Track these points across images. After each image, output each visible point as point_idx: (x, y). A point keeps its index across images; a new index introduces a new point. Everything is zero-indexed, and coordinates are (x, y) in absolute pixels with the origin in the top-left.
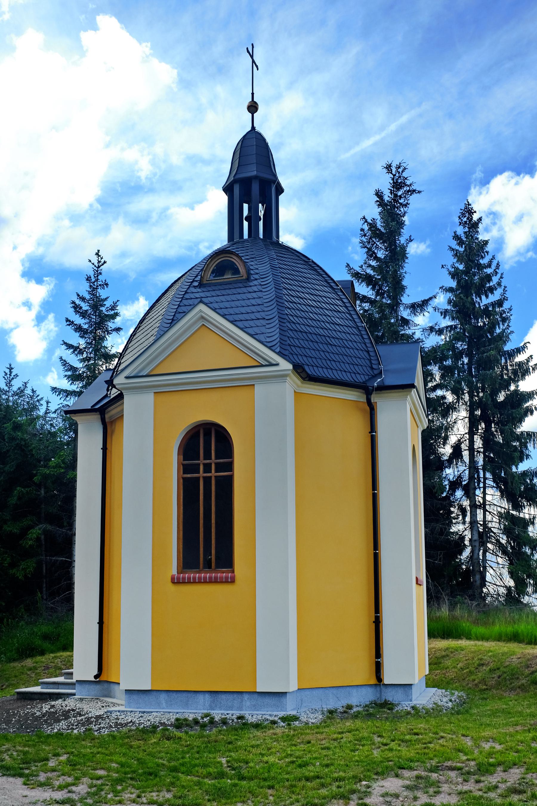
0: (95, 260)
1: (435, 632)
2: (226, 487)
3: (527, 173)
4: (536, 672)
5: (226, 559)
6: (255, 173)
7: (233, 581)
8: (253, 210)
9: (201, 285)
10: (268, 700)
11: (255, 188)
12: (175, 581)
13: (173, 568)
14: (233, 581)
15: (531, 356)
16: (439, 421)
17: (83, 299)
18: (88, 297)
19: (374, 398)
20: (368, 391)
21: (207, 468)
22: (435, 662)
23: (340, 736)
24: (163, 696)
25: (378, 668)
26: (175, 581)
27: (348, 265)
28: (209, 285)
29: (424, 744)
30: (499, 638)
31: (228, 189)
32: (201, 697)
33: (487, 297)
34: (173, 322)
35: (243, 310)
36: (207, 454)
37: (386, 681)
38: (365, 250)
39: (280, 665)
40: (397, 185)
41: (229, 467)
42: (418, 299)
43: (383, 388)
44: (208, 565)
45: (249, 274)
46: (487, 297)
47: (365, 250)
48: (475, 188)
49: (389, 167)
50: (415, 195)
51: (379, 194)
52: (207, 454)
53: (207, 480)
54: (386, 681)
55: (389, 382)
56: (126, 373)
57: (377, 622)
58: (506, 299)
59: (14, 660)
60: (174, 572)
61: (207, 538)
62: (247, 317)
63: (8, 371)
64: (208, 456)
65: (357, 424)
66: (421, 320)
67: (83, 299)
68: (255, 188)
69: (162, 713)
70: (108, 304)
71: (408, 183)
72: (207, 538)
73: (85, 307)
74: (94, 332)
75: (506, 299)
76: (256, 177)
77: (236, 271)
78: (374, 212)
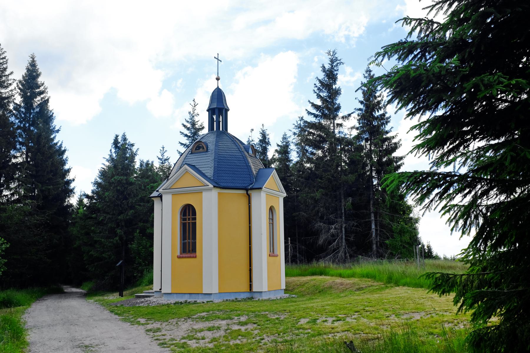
0: (193, 103)
1: (287, 275)
2: (194, 224)
5: (194, 250)
6: (216, 106)
7: (196, 257)
8: (218, 118)
9: (191, 154)
10: (206, 296)
11: (217, 111)
12: (179, 257)
13: (178, 253)
14: (196, 257)
15: (401, 140)
17: (188, 122)
18: (190, 121)
19: (249, 192)
20: (247, 190)
22: (287, 284)
24: (175, 295)
25: (251, 286)
26: (179, 257)
27: (309, 101)
28: (194, 153)
30: (363, 276)
31: (208, 111)
32: (186, 295)
33: (378, 111)
34: (181, 167)
35: (203, 164)
36: (188, 213)
38: (316, 94)
39: (211, 284)
40: (332, 61)
41: (195, 219)
42: (346, 113)
43: (252, 189)
44: (189, 251)
45: (207, 149)
46: (378, 111)
47: (316, 94)
48: (284, 150)
49: (329, 53)
50: (342, 65)
51: (323, 67)
52: (188, 213)
54: (254, 290)
55: (255, 187)
56: (162, 188)
58: (386, 113)
59: (147, 285)
61: (189, 244)
62: (204, 166)
63: (162, 149)
64: (189, 215)
65: (245, 201)
67: (188, 122)
68: (217, 111)
69: (172, 300)
70: (199, 123)
71: (339, 59)
72: (189, 244)
73: (189, 125)
74: (193, 136)
75: (386, 113)
76: (216, 108)
77: (203, 149)
78: (322, 76)
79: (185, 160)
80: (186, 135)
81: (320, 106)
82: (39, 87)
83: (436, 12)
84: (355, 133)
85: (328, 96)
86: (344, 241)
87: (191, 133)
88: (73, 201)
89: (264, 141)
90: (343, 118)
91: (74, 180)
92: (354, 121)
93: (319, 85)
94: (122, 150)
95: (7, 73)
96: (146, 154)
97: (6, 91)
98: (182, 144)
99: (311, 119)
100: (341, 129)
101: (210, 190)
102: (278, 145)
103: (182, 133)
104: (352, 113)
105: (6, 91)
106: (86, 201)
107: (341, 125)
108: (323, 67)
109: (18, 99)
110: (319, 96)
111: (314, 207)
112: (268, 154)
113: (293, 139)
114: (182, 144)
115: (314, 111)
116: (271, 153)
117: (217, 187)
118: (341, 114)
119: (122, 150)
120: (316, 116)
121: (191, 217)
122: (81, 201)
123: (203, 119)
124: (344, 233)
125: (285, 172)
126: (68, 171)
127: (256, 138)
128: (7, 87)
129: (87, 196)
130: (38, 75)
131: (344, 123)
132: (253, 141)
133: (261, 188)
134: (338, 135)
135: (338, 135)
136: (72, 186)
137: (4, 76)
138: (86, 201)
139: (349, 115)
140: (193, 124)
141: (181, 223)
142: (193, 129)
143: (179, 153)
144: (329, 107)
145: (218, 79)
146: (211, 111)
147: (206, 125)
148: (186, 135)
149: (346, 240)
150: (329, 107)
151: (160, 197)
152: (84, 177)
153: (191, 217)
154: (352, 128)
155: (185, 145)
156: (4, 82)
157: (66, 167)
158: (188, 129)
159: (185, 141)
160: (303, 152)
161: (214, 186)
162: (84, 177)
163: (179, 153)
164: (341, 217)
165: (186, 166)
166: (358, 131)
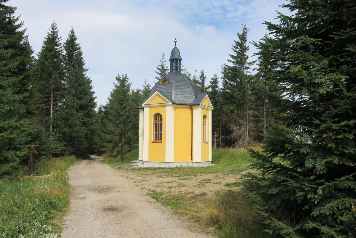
2: (161, 124)
3: (81, 61)
4: (348, 170)
5: (161, 139)
11: (175, 61)
13: (153, 139)
16: (219, 143)
17: (160, 66)
21: (159, 121)
23: (342, 34)
26: (152, 142)
29: (168, 188)
36: (158, 118)
37: (194, 161)
41: (162, 121)
44: (158, 139)
48: (214, 82)
51: (238, 34)
52: (158, 118)
53: (158, 124)
57: (192, 156)
60: (153, 140)
61: (158, 135)
64: (159, 119)
66: (252, 67)
68: (175, 61)
72: (158, 135)
73: (160, 68)
79: (157, 88)
80: (158, 73)
81: (236, 57)
82: (76, 45)
83: (142, 138)
84: (256, 72)
85: (241, 51)
86: (247, 135)
87: (161, 72)
88: (96, 109)
89: (203, 77)
90: (249, 63)
91: (96, 98)
92: (256, 66)
93: (235, 45)
94: (123, 82)
95: (58, 37)
96: (136, 85)
97: (58, 47)
98: (156, 78)
99: (231, 65)
100: (248, 70)
101: (170, 105)
102: (271, 27)
103: (156, 72)
104: (255, 61)
105: (58, 47)
106: (103, 109)
107: (248, 68)
108: (238, 34)
109: (65, 53)
110: (235, 51)
111: (231, 115)
112: (231, 66)
113: (220, 75)
114: (156, 78)
115: (232, 60)
116: (207, 83)
117: (174, 104)
118: (248, 61)
119: (123, 82)
120: (233, 62)
121: (160, 120)
122: (100, 109)
123: (167, 65)
124: (247, 130)
125: (213, 95)
126: (94, 92)
127: (198, 75)
128: (58, 45)
129: (104, 107)
130: (75, 39)
131: (250, 67)
132: (160, 61)
133: (199, 105)
134: (245, 74)
135: (245, 74)
136: (95, 101)
137: (57, 39)
138: (103, 109)
139: (254, 62)
140: (163, 67)
141: (154, 123)
142: (163, 69)
143: (155, 83)
144: (240, 56)
145: (175, 42)
146: (172, 60)
147: (169, 68)
148: (158, 73)
149: (248, 134)
150: (240, 56)
151: (143, 108)
152: (102, 96)
153: (160, 120)
154: (254, 69)
155: (158, 78)
156: (57, 42)
157: (92, 90)
158: (160, 70)
159: (159, 76)
160: (225, 83)
161: (173, 103)
162: (102, 96)
163: (155, 83)
164: (246, 121)
165: (157, 92)
166: (258, 71)
